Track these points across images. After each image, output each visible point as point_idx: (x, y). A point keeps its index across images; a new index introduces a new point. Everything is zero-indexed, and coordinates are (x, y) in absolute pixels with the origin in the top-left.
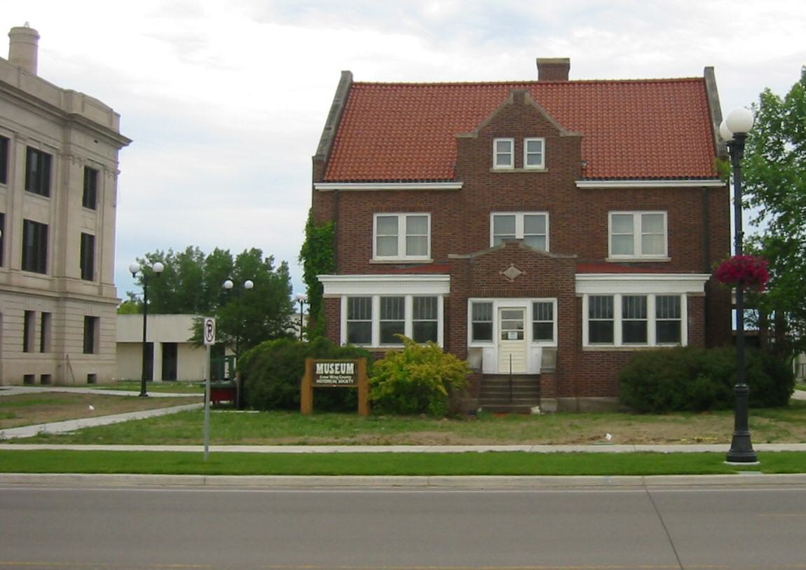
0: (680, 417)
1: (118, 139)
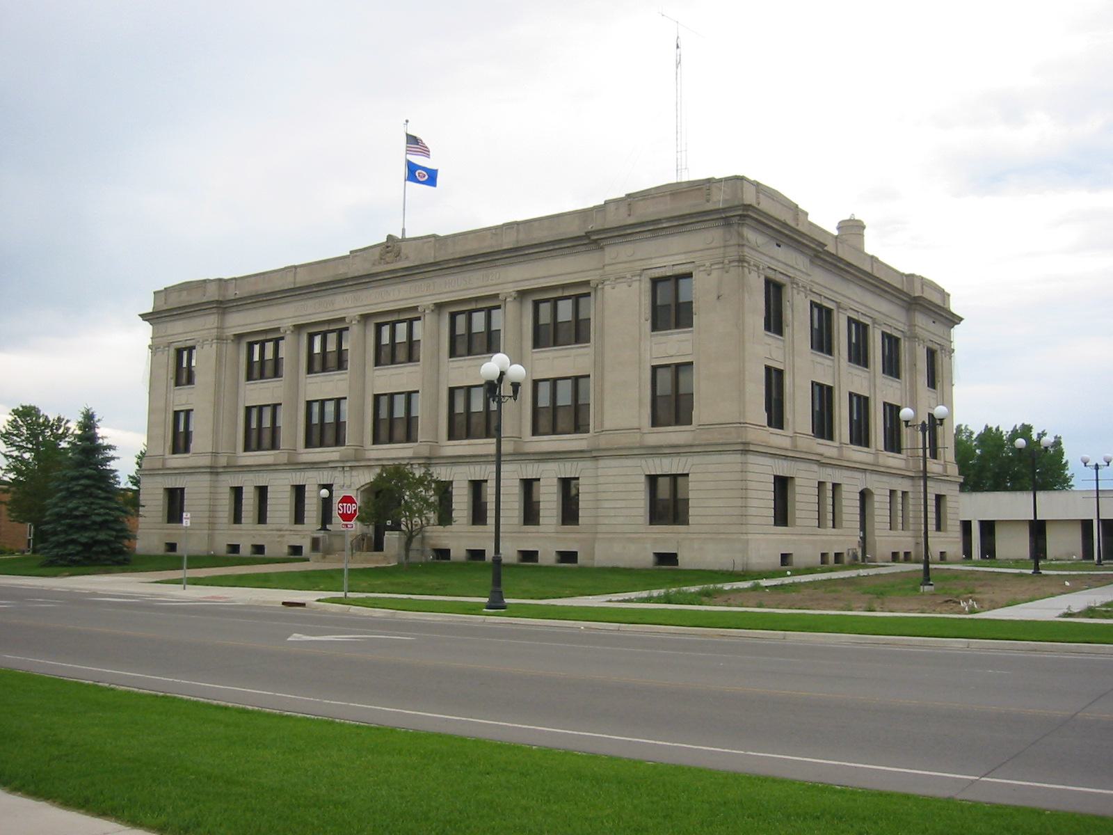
1: (951, 318)
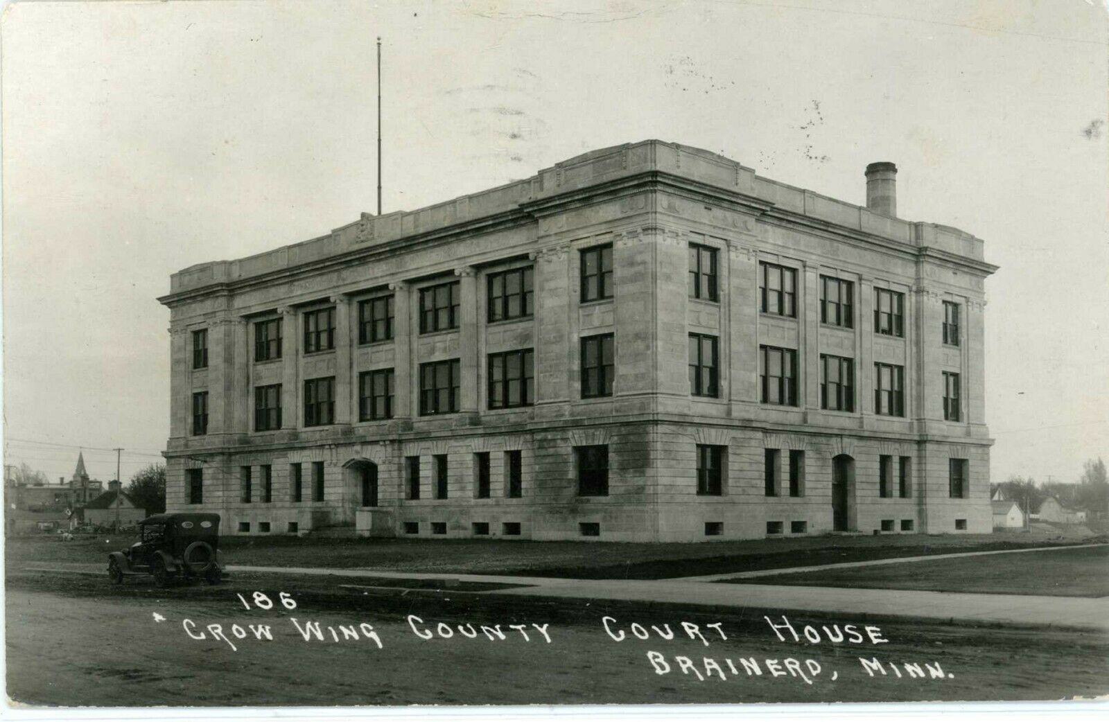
0: (419, 322)
